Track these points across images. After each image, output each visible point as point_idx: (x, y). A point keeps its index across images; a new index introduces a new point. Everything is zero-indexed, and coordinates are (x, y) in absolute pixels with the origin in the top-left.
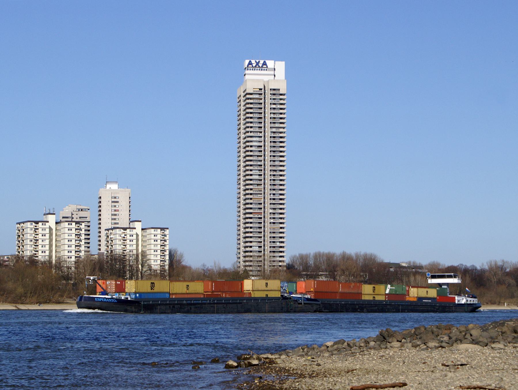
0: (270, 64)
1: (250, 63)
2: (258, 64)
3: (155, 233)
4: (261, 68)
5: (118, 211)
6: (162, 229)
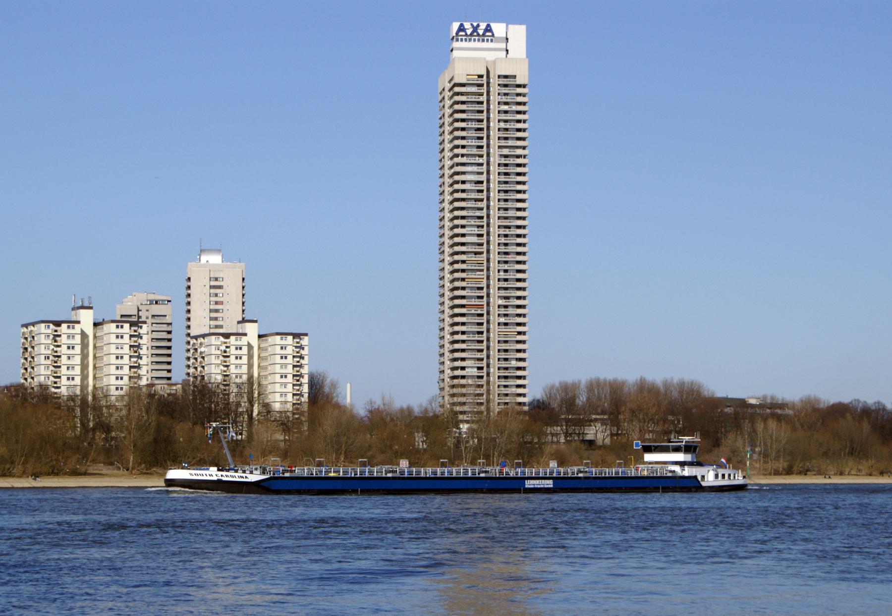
0: (499, 29)
1: (461, 28)
2: (475, 29)
3: (283, 342)
4: (482, 38)
5: (222, 303)
6: (296, 336)
